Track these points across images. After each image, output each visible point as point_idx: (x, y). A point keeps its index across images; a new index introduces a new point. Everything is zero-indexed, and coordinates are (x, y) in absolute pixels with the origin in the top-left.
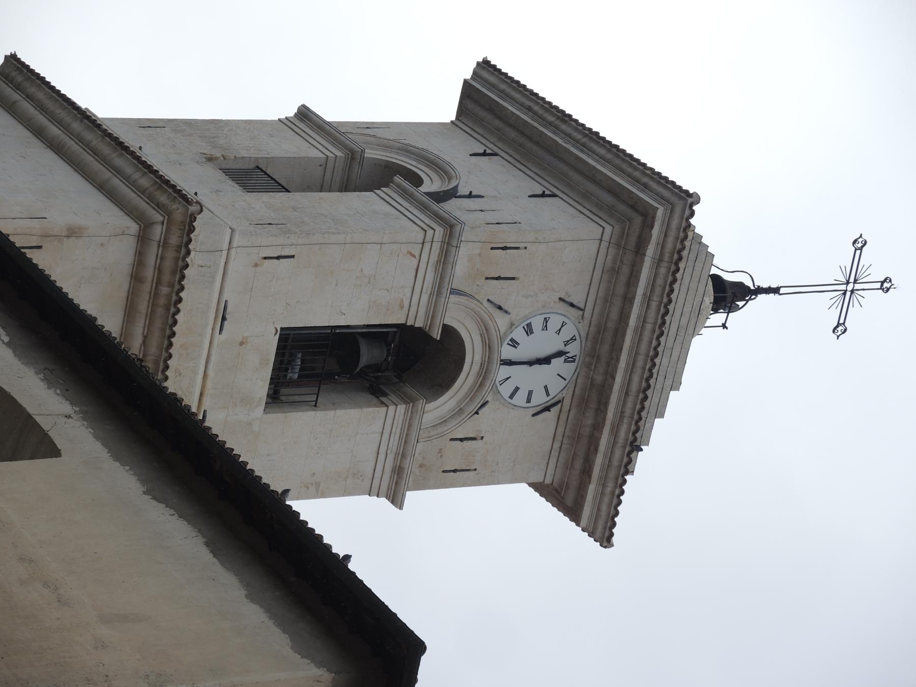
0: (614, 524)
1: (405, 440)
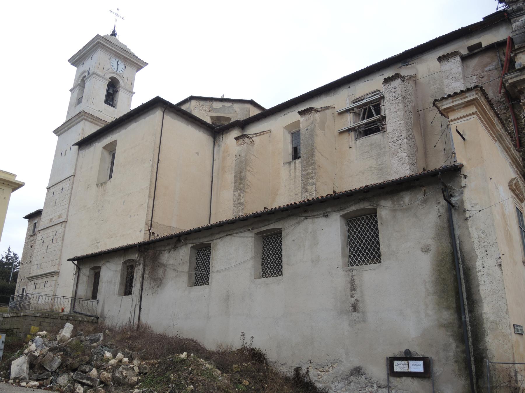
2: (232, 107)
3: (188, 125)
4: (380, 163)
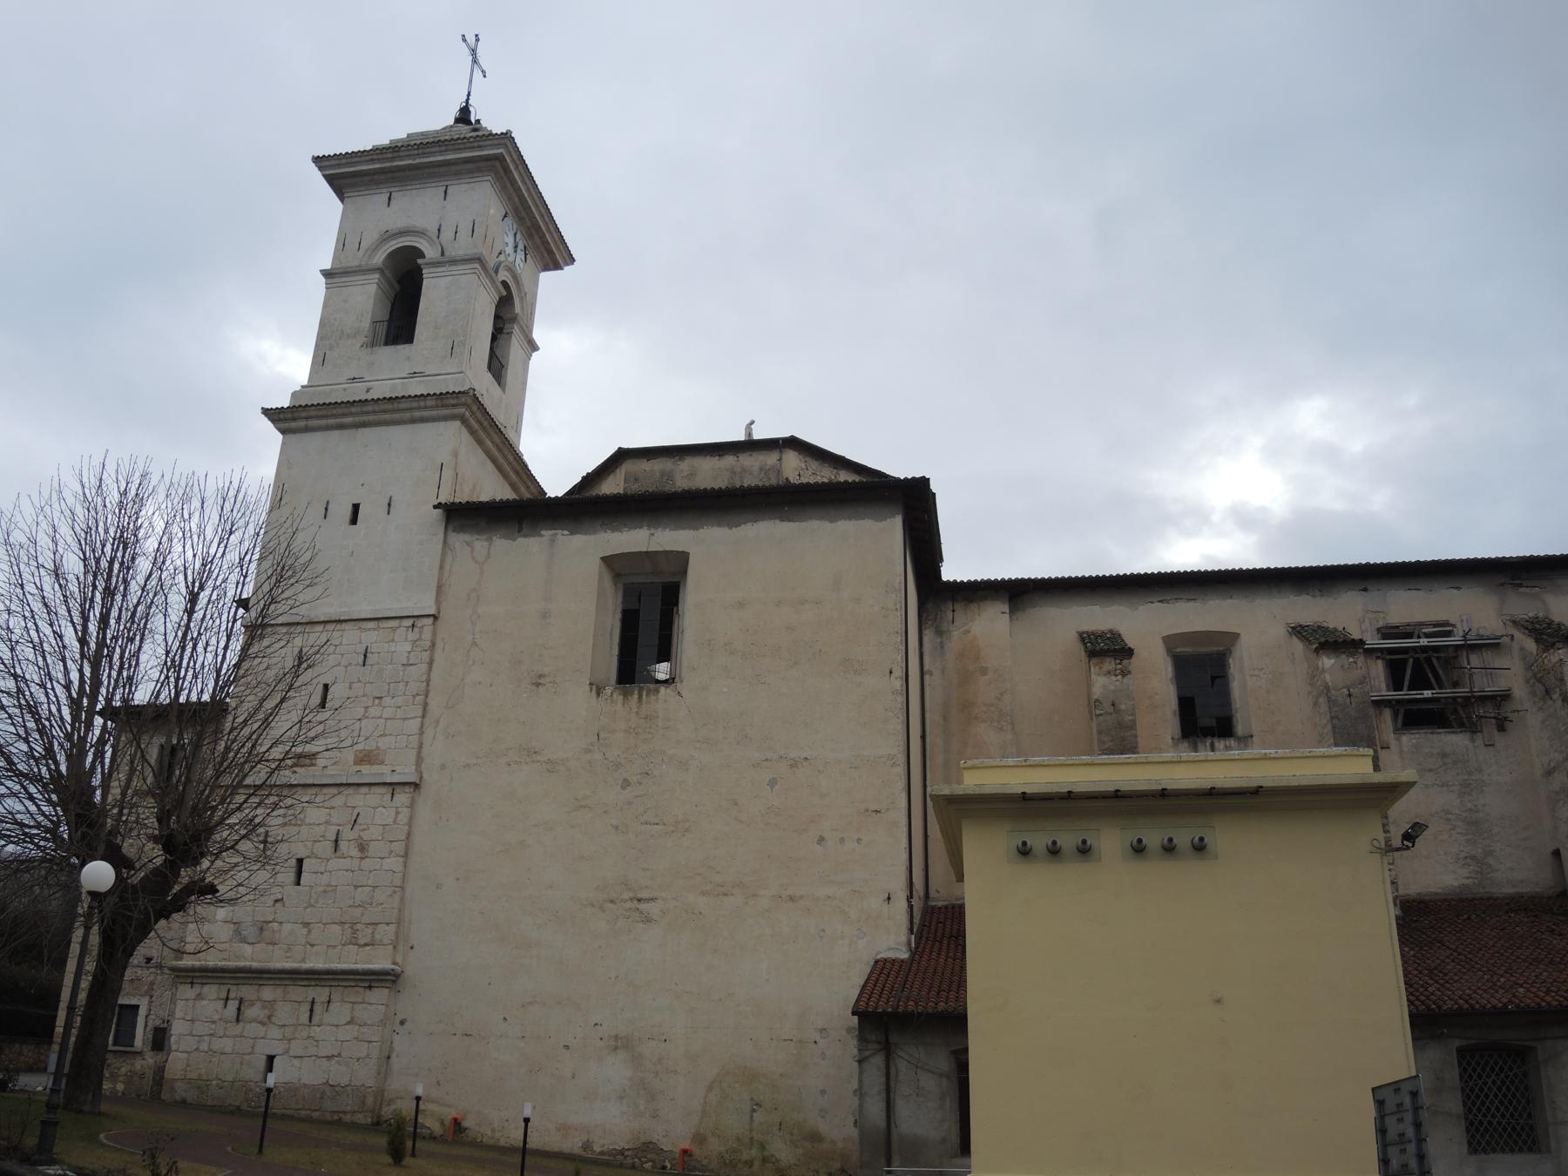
4: (1469, 805)
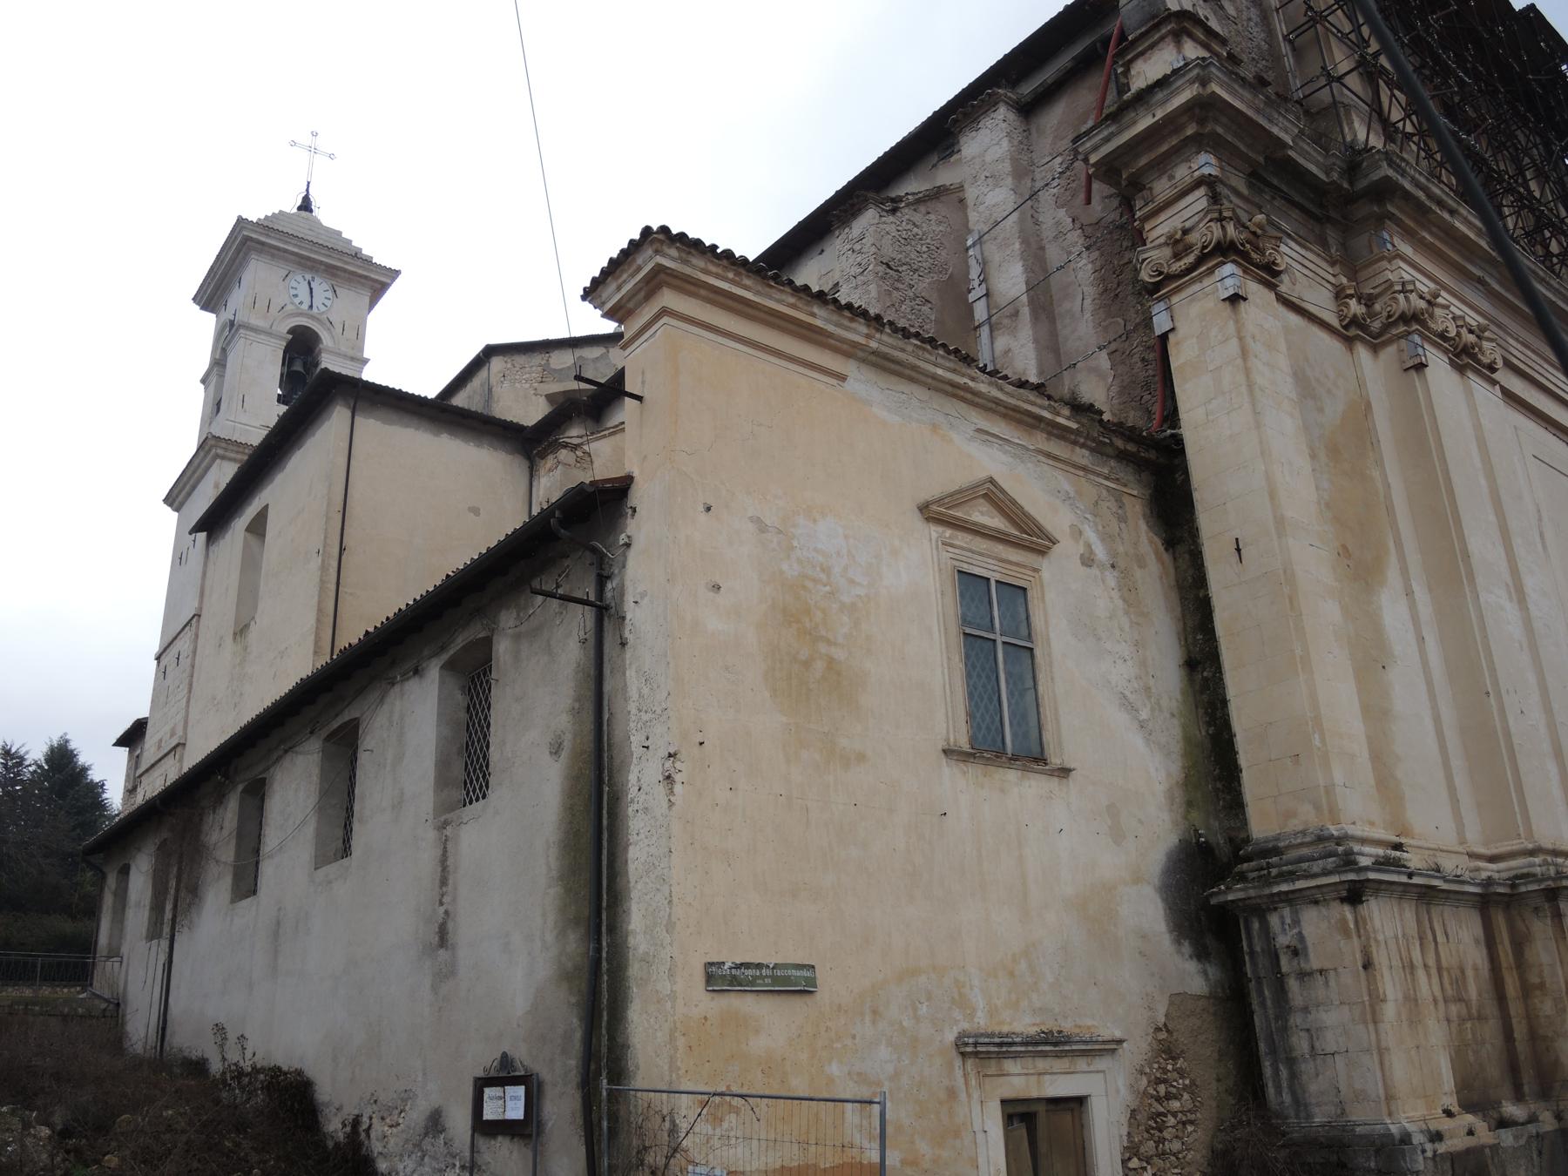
0: (682, 236)
1: (339, 355)
2: (604, 357)
3: (437, 434)
